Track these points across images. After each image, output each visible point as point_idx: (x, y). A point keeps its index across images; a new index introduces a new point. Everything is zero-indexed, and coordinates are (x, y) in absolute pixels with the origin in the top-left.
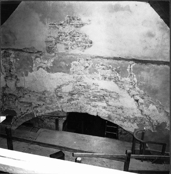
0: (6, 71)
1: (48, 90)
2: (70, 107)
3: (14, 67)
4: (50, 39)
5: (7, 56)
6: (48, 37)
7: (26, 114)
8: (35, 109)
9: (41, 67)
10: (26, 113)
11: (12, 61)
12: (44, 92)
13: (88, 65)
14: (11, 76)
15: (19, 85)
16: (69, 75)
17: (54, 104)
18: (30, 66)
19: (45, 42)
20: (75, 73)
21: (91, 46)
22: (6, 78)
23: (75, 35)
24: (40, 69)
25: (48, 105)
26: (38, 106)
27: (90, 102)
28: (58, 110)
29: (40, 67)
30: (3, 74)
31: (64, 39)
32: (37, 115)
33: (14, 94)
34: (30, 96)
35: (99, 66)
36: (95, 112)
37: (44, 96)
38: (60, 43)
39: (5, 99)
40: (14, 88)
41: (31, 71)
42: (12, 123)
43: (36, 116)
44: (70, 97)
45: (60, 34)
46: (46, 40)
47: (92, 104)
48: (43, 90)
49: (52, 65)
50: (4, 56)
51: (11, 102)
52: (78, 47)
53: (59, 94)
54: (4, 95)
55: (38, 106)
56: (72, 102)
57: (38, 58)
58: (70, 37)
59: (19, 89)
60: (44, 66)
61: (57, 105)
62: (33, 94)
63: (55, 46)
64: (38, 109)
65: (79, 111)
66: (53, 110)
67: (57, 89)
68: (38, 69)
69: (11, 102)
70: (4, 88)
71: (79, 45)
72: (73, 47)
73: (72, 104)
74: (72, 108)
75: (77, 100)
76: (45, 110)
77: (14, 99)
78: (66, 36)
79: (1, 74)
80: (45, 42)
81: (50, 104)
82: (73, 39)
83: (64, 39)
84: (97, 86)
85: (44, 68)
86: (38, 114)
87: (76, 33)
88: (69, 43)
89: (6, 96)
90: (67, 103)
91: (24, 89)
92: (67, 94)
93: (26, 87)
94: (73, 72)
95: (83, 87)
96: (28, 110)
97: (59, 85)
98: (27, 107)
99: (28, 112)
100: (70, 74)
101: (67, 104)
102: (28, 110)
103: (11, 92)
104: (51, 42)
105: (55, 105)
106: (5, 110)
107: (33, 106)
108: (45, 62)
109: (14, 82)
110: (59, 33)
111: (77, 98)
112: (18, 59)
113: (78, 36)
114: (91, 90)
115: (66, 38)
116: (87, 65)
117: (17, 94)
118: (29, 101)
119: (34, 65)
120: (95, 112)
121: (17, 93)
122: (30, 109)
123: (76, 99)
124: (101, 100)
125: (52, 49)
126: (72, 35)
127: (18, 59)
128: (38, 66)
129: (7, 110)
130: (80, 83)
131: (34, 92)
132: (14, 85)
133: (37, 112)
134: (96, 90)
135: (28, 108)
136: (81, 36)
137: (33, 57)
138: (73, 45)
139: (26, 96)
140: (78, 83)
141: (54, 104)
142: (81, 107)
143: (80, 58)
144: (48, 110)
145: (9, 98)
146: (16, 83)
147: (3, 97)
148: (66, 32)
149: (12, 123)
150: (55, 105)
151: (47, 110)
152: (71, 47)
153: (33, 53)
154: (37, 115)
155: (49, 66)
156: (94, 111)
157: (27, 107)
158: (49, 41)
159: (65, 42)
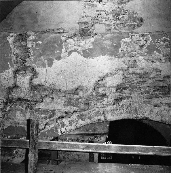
0: (17, 62)
1: (84, 85)
2: (119, 111)
3: (32, 54)
4: (85, 20)
5: (22, 40)
6: (83, 17)
7: (43, 131)
8: (59, 122)
9: (75, 51)
10: (43, 129)
11: (29, 46)
12: (77, 89)
13: (144, 43)
14: (25, 69)
15: (36, 82)
16: (117, 59)
17: (92, 110)
18: (58, 51)
19: (78, 23)
20: (126, 55)
21: (141, 25)
22: (16, 72)
23: (119, 13)
24: (74, 54)
25: (81, 113)
26: (64, 115)
27: (149, 100)
28: (99, 117)
29: (72, 51)
30: (12, 66)
31: (104, 18)
32: (61, 132)
33: (26, 97)
34: (52, 98)
35: (160, 43)
36: (159, 114)
37: (76, 97)
38: (100, 23)
39: (8, 108)
40: (28, 88)
41: (59, 58)
42: (14, 152)
43: (60, 134)
44: (118, 94)
45: (99, 13)
46: (80, 21)
47: (152, 103)
48: (76, 86)
49: (92, 47)
50: (19, 39)
51: (18, 113)
52: (125, 27)
53: (101, 90)
54: (9, 101)
55: (64, 115)
56: (121, 103)
57: (70, 39)
58: (113, 15)
59: (34, 88)
60: (79, 49)
61: (97, 110)
62: (58, 95)
63: (93, 28)
64: (64, 120)
65: (113, 120)
66: (90, 119)
67: (99, 82)
68: (69, 54)
69: (18, 113)
70: (10, 90)
71: (126, 25)
72: (117, 28)
73: (122, 106)
74: (121, 113)
75: (130, 99)
76: (77, 121)
77: (25, 106)
78: (107, 15)
79: (10, 66)
80: (78, 23)
81: (86, 110)
82: (117, 18)
83: (104, 18)
84: (159, 73)
85: (79, 53)
86: (63, 130)
87: (121, 10)
88: (112, 23)
89: (10, 103)
90: (114, 105)
91: (44, 87)
92: (114, 90)
93: (47, 85)
94: (124, 54)
95: (138, 76)
96: (47, 124)
97: (102, 75)
98: (45, 118)
99: (47, 127)
100: (119, 58)
101: (113, 108)
102: (47, 124)
103: (22, 95)
104: (86, 23)
105: (95, 110)
106: (5, 128)
107: (56, 117)
108: (81, 44)
109: (28, 78)
110: (97, 11)
111: (130, 95)
112: (40, 42)
113: (124, 14)
114: (150, 79)
115: (107, 17)
116: (142, 42)
117: (32, 97)
118: (50, 107)
119: (64, 49)
120: (159, 114)
121: (31, 95)
122: (50, 123)
123: (128, 97)
124: (166, 94)
125: (88, 32)
126: (115, 13)
127: (40, 42)
128: (69, 50)
129: (9, 128)
130: (134, 69)
131: (60, 91)
132: (28, 82)
133: (63, 125)
134: (158, 79)
135: (47, 120)
136: (127, 13)
137: (63, 38)
138: (117, 25)
139: (47, 100)
140: (131, 70)
141: (92, 110)
142: (136, 108)
143: (133, 34)
144: (82, 120)
145: (17, 105)
146: (31, 79)
147: (6, 104)
148: (107, 10)
149: (14, 152)
150: (95, 110)
151: (80, 120)
152: (115, 28)
153: (63, 32)
154: (61, 132)
155: (87, 48)
156: (157, 113)
157: (45, 118)
158: (84, 22)
159: (107, 22)
